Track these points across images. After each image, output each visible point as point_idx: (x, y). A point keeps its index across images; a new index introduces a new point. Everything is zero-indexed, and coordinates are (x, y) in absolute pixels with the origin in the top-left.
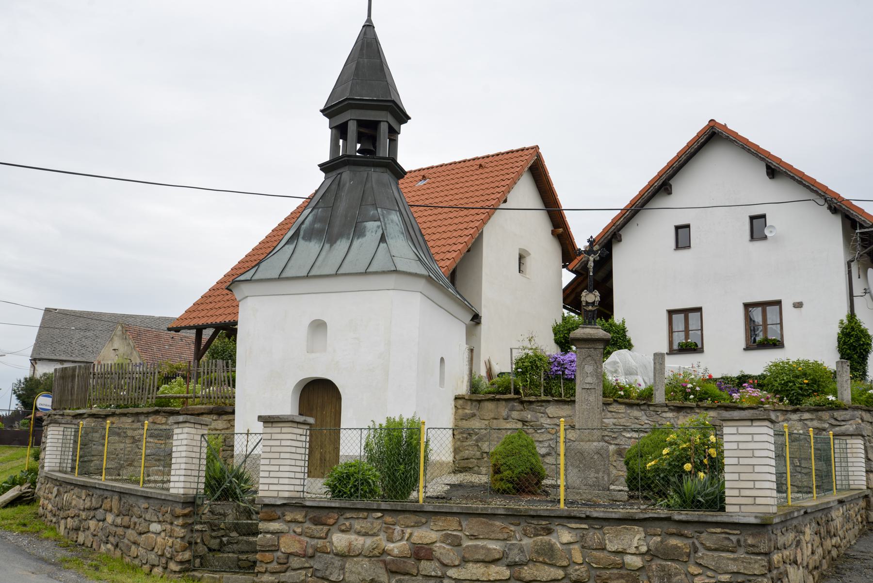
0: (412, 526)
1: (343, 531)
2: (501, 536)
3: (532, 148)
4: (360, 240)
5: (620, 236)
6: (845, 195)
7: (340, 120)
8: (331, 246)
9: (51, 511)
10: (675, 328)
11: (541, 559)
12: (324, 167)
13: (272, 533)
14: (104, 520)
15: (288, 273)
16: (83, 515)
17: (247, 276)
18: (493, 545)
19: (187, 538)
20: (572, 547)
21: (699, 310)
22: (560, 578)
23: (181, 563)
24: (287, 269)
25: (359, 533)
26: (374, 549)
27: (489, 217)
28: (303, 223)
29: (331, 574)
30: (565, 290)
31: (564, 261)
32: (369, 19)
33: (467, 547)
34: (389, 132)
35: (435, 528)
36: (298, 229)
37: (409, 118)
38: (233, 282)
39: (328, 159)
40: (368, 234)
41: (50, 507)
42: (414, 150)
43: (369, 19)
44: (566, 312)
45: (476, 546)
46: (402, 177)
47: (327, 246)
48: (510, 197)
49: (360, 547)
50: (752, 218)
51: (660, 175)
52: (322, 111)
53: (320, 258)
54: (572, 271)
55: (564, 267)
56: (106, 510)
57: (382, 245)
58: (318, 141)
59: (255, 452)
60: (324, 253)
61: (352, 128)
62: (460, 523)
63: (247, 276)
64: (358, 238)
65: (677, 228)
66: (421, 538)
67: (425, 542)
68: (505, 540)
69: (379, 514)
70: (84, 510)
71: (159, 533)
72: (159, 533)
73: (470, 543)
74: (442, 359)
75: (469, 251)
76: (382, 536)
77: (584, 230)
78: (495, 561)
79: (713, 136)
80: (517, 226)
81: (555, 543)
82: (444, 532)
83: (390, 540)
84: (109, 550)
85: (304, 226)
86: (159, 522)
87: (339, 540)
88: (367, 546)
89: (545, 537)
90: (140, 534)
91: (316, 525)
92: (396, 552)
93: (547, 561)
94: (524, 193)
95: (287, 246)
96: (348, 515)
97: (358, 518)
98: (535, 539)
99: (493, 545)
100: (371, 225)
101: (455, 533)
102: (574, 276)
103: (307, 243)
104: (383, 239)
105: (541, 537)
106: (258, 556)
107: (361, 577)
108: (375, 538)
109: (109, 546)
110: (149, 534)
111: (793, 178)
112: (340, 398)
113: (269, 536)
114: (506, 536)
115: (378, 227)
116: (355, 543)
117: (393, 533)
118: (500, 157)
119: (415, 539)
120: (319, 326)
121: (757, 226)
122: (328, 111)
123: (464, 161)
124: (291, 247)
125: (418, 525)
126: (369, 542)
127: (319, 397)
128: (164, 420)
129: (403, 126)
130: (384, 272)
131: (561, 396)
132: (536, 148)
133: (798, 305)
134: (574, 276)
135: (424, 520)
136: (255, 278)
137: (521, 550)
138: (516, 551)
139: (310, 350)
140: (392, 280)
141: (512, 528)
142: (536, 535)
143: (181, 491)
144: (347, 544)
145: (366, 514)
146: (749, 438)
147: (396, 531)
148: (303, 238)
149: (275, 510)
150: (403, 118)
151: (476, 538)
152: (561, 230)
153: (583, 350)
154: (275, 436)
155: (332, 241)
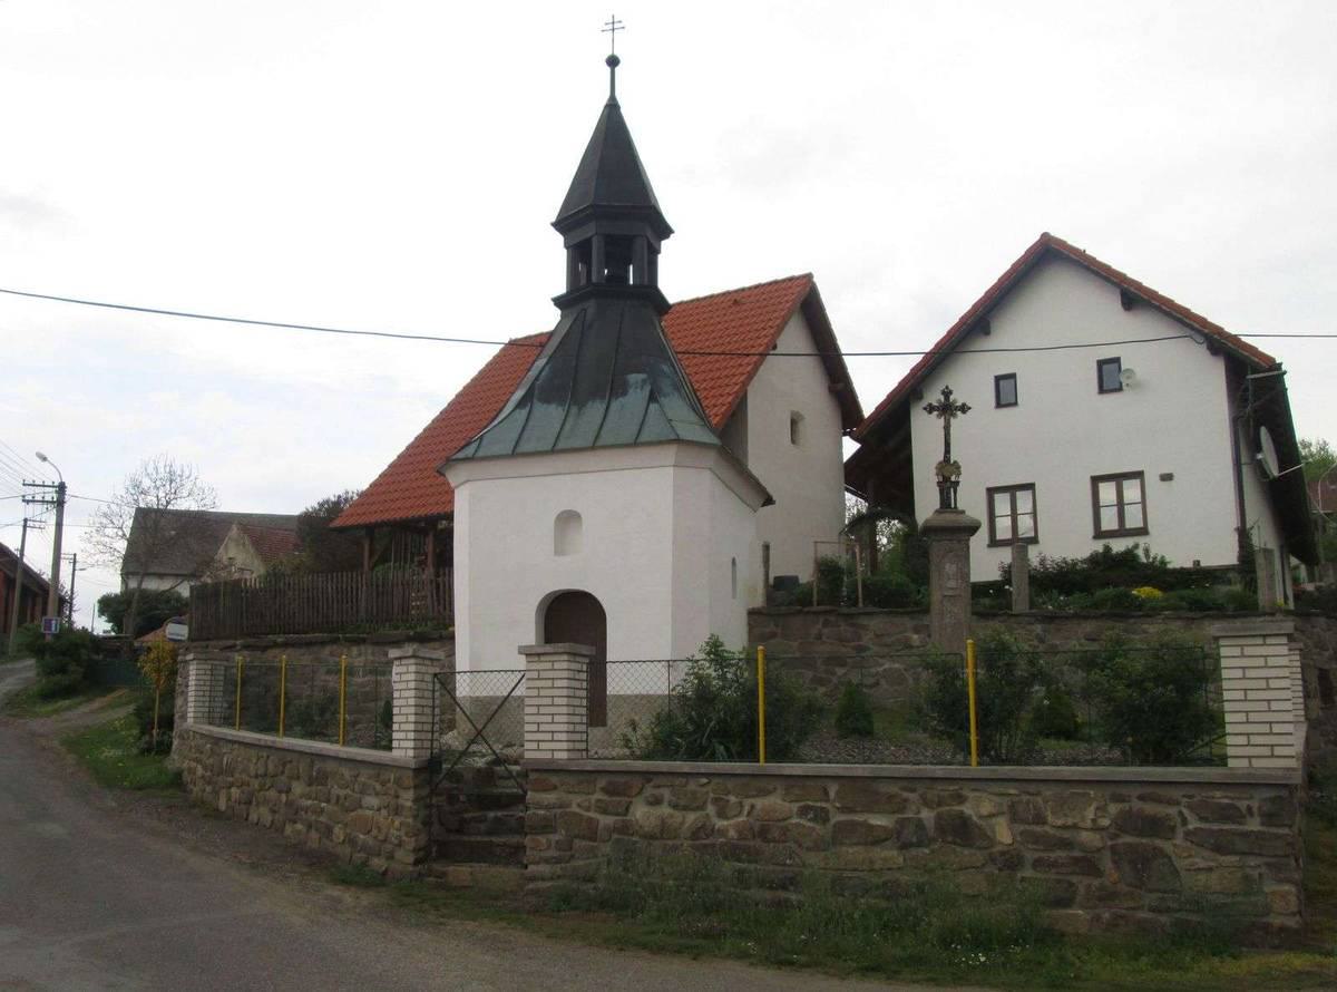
6: (1231, 329)
8: (580, 409)
9: (203, 777)
10: (998, 512)
12: (558, 302)
13: (547, 807)
14: (288, 791)
15: (524, 447)
16: (256, 784)
17: (469, 451)
18: (878, 821)
20: (994, 820)
21: (1030, 487)
22: (979, 864)
24: (521, 443)
32: (613, 98)
33: (839, 823)
41: (200, 770)
42: (682, 275)
46: (666, 313)
47: (574, 410)
50: (1101, 364)
53: (567, 427)
55: (845, 434)
56: (290, 778)
57: (653, 407)
58: (551, 267)
59: (517, 693)
60: (570, 420)
65: (998, 379)
69: (705, 780)
70: (257, 776)
72: (379, 810)
74: (734, 560)
77: (872, 387)
79: (1048, 256)
80: (786, 381)
83: (722, 814)
84: (299, 832)
86: (377, 794)
94: (794, 338)
98: (940, 809)
99: (878, 821)
100: (634, 378)
105: (947, 808)
106: (528, 841)
109: (299, 826)
110: (360, 812)
111: (1158, 309)
112: (604, 614)
115: (644, 381)
116: (670, 821)
121: (1110, 377)
122: (561, 224)
124: (524, 412)
127: (572, 620)
130: (660, 443)
131: (855, 604)
133: (1167, 477)
136: (480, 454)
137: (920, 825)
144: (659, 823)
145: (684, 780)
146: (1261, 662)
148: (540, 400)
149: (547, 772)
150: (665, 231)
151: (851, 810)
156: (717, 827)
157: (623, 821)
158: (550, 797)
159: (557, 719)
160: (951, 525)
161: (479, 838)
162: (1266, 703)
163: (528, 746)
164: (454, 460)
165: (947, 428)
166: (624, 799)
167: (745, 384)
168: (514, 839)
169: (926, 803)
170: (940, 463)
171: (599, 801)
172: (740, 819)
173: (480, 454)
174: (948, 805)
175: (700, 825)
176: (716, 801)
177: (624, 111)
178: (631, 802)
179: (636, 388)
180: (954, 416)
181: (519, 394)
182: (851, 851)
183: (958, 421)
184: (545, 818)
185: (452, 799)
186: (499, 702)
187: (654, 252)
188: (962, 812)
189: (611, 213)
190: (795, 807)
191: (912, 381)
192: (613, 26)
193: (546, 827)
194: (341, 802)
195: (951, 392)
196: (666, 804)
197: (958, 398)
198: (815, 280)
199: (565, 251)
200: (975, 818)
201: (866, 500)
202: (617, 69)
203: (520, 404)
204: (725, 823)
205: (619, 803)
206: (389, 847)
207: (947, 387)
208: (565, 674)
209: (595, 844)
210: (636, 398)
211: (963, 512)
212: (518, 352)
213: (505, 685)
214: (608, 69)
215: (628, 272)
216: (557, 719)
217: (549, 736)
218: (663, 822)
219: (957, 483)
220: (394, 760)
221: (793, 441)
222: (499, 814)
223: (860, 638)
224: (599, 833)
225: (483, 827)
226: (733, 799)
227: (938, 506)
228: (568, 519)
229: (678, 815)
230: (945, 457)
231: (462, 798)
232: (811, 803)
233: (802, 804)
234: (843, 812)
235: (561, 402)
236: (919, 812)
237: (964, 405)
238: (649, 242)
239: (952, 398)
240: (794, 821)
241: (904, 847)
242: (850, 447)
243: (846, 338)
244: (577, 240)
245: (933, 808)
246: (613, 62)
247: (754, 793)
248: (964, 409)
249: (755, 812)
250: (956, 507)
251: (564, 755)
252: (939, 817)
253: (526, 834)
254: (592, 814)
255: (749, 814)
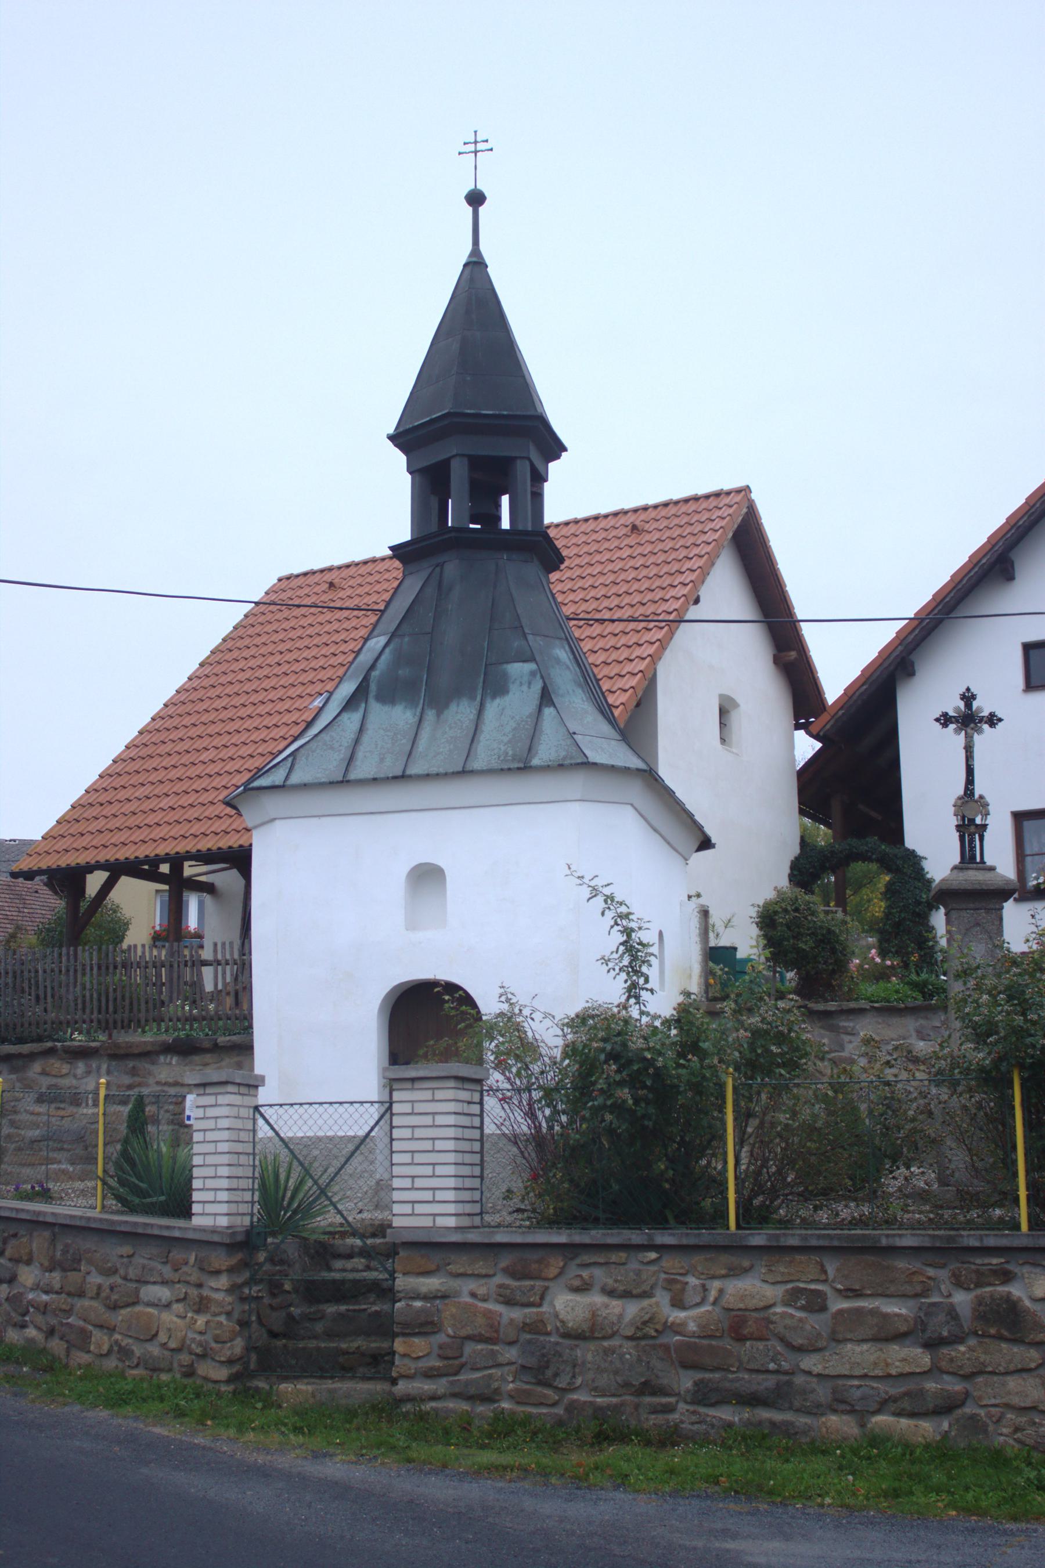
0: (724, 1276)
1: (576, 1290)
2: (908, 1289)
3: (738, 491)
4: (498, 701)
5: (912, 664)
7: (433, 455)
8: (439, 714)
11: (993, 1331)
13: (425, 1298)
18: (893, 1308)
19: (236, 1315)
22: (1033, 1365)
23: (230, 1362)
25: (611, 1293)
26: (645, 1323)
27: (672, 633)
28: (373, 667)
29: (556, 1375)
30: (802, 773)
31: (797, 717)
32: (476, 251)
33: (841, 1312)
34: (532, 480)
35: (770, 1278)
36: (366, 679)
37: (565, 449)
38: (249, 789)
39: (407, 537)
40: (513, 688)
43: (476, 251)
44: (807, 821)
45: (858, 1311)
46: (556, 568)
47: (430, 715)
48: (704, 592)
49: (615, 1319)
51: (994, 540)
52: (391, 438)
54: (816, 737)
55: (798, 727)
56: (16, 1261)
57: (548, 712)
61: (459, 474)
62: (822, 1266)
63: (276, 777)
64: (494, 697)
66: (742, 1298)
67: (751, 1306)
68: (916, 1296)
69: (653, 1255)
71: (168, 1306)
73: (845, 1305)
75: (638, 705)
76: (662, 1299)
77: (839, 666)
78: (898, 1337)
80: (714, 658)
81: (1020, 1299)
82: (790, 1286)
83: (678, 1303)
85: (375, 674)
86: (164, 1283)
87: (566, 1305)
88: (628, 1318)
89: (1000, 1289)
90: (115, 1307)
91: (519, 1279)
92: (692, 1327)
93: (1006, 1333)
94: (725, 591)
95: (345, 716)
96: (586, 1258)
97: (606, 1263)
98: (979, 1291)
99: (893, 1308)
100: (518, 669)
101: (813, 1286)
102: (818, 745)
103: (386, 708)
104: (546, 698)
105: (988, 1289)
107: (619, 1379)
108: (646, 1303)
110: (138, 1308)
113: (418, 1304)
114: (919, 1288)
115: (533, 674)
117: (683, 1290)
118: (672, 510)
119: (730, 1299)
120: (427, 877)
123: (596, 518)
124: (351, 721)
125: (735, 1272)
126: (632, 1310)
128: (65, 1068)
129: (552, 466)
132: (746, 490)
134: (818, 745)
135: (746, 1263)
136: (294, 779)
137: (952, 1313)
138: (942, 1317)
139: (412, 925)
140: (576, 783)
141: (931, 1272)
142: (978, 1285)
143: (223, 1222)
144: (588, 1315)
147: (689, 1288)
149: (431, 1249)
150: (554, 448)
151: (857, 1294)
152: (793, 654)
153: (964, 914)
154: (420, 1108)
155: (438, 701)
156: (671, 1319)
157: (537, 1313)
158: (432, 1283)
159: (440, 1170)
160: (978, 887)
161: (312, 1344)
162: (410, 1180)
163: (397, 1209)
164: (253, 789)
165: (969, 750)
166: (539, 1284)
167: (654, 659)
168: (376, 1344)
169: (959, 1283)
170: (960, 798)
171: (500, 1286)
172: (702, 1309)
173: (294, 779)
174: (990, 1285)
175: (646, 1317)
176: (670, 1284)
177: (495, 273)
178: (547, 1288)
179: (521, 684)
180: (980, 731)
181: (348, 688)
182: (858, 1349)
183: (985, 739)
184: (422, 1310)
185: (275, 1288)
186: (357, 1141)
187: (539, 478)
188: (1010, 1293)
189: (474, 424)
190: (779, 1291)
191: (900, 648)
192: (476, 147)
193: (425, 1326)
194: (103, 1295)
195: (974, 697)
196: (597, 1288)
197: (984, 705)
198: (753, 496)
199: (409, 477)
200: (1027, 1303)
201: (828, 825)
202: (481, 209)
203: (350, 704)
204: (683, 1314)
205: (533, 1287)
206: (185, 1358)
207: (968, 689)
208: (452, 1107)
209: (496, 1348)
210: (515, 704)
211: (992, 869)
212: (297, 602)
213: (361, 1121)
214: (470, 210)
215: (498, 506)
216: (440, 1170)
217: (427, 1196)
218: (594, 1315)
219: (984, 827)
220: (196, 1229)
221: (723, 740)
222: (343, 1308)
223: (842, 1048)
224: (502, 1330)
225: (319, 1327)
226: (692, 1281)
227: (957, 860)
228: (427, 877)
229: (616, 1305)
230: (966, 789)
231: (287, 1287)
232: (802, 1285)
233: (790, 1286)
234: (847, 1297)
235: (411, 701)
236: (950, 1295)
237: (992, 715)
238: (532, 466)
239: (975, 705)
240: (779, 1309)
241: (932, 1345)
242: (806, 747)
243: (803, 598)
244: (425, 463)
245: (968, 1289)
246: (476, 199)
247: (723, 1272)
248: (993, 720)
249: (723, 1302)
250: (982, 861)
251: (451, 1222)
252: (980, 1301)
253: (395, 1335)
254: (491, 1306)
255: (714, 1303)
